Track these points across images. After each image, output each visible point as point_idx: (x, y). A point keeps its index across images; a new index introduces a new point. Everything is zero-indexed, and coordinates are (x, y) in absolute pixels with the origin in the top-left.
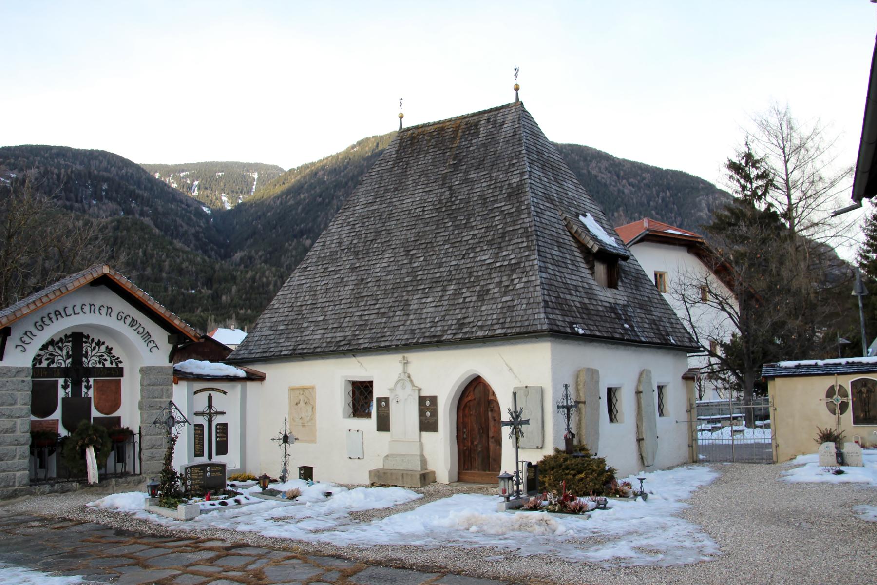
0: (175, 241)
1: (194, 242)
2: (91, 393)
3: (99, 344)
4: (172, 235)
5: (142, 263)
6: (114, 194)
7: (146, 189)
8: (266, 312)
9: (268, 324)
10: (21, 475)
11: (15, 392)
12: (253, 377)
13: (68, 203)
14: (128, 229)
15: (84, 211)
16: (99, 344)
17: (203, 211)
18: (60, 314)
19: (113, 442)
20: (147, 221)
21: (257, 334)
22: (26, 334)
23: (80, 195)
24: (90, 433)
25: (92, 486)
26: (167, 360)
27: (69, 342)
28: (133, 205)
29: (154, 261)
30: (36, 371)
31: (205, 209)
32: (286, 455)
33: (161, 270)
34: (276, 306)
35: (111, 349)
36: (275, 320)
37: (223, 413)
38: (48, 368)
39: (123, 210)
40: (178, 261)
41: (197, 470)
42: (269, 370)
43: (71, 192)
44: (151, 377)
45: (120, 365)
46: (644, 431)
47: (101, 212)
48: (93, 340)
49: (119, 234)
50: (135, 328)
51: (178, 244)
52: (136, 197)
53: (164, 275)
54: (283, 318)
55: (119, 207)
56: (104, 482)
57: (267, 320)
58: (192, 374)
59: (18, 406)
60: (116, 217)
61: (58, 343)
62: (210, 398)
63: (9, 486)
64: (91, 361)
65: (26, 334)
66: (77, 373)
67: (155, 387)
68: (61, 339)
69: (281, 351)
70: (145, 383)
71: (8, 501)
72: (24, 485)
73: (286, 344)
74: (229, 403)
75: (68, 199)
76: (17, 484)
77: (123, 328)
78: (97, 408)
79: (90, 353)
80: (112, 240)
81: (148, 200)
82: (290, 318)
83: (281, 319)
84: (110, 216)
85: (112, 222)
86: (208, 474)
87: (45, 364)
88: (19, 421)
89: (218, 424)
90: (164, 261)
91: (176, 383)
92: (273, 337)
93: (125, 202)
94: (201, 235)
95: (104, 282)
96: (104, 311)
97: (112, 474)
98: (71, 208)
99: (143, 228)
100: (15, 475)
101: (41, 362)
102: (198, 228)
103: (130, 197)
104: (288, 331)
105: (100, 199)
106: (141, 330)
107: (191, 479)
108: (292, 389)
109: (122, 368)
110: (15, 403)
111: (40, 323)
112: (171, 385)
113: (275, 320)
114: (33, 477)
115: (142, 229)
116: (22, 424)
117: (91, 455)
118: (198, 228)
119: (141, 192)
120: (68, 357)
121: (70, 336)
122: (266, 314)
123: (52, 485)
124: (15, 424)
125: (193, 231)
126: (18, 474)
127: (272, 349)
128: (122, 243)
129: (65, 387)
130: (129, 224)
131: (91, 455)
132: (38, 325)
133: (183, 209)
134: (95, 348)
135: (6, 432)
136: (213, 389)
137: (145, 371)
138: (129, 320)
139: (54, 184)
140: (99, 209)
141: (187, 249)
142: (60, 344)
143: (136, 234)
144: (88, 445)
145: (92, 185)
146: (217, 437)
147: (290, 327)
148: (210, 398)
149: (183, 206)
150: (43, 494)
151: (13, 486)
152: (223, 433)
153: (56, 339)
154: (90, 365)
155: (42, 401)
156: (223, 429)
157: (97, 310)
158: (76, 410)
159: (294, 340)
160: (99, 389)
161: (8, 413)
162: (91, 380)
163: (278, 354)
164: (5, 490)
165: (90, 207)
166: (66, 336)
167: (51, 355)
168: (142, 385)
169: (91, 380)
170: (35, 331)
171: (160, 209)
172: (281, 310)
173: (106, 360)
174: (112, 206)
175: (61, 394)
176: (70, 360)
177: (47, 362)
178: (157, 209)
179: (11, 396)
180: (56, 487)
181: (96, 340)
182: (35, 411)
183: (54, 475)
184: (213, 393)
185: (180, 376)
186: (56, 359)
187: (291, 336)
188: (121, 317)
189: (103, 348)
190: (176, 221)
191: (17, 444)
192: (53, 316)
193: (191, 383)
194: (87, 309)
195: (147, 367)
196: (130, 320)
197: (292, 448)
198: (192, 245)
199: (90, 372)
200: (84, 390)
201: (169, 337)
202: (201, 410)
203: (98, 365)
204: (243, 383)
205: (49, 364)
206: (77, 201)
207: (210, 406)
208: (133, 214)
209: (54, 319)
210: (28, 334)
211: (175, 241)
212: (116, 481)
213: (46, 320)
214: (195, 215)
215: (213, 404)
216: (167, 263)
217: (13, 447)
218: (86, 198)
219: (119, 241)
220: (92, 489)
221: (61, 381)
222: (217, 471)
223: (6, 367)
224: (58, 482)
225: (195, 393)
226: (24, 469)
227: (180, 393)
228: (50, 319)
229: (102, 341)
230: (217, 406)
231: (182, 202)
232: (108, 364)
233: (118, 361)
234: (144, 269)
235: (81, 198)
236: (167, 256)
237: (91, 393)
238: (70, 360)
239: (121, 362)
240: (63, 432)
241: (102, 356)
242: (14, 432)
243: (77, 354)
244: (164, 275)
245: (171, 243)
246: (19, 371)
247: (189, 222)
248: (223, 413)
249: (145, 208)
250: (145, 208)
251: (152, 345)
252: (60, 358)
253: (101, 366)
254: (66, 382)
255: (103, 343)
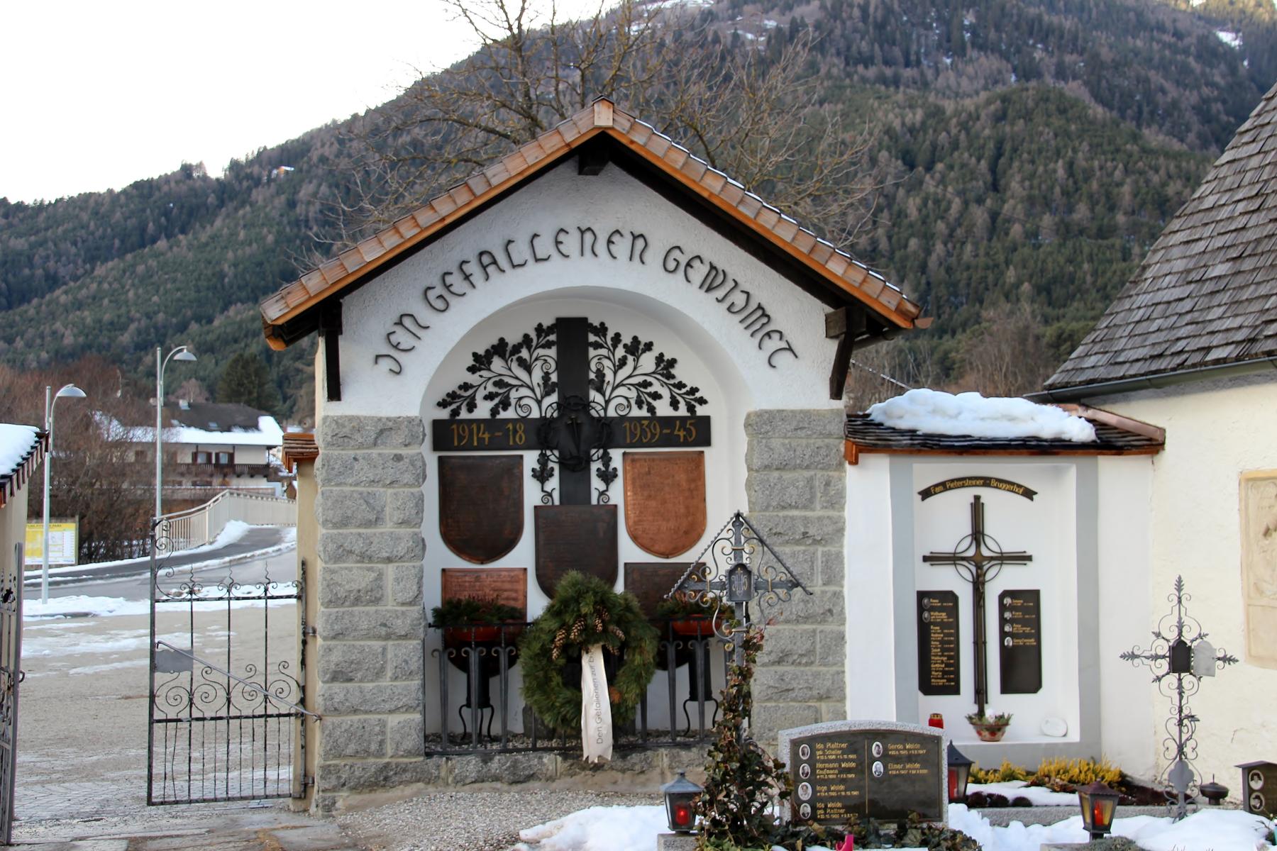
0: (1146, 132)
1: (1196, 127)
2: (617, 494)
3: (636, 348)
4: (1138, 118)
5: (1065, 193)
6: (992, 35)
7: (1068, 10)
8: (1176, 224)
9: (1179, 265)
10: (402, 726)
11: (378, 490)
12: (1110, 442)
13: (889, 72)
14: (1028, 116)
15: (925, 85)
16: (636, 348)
17: (1221, 43)
18: (495, 262)
19: (663, 638)
20: (1074, 89)
21: (1145, 299)
22: (400, 323)
23: (914, 48)
24: (585, 610)
25: (597, 767)
26: (825, 389)
27: (548, 345)
28: (1038, 55)
29: (1095, 185)
30: (443, 434)
31: (1226, 37)
32: (1184, 719)
33: (1112, 208)
34: (1208, 202)
35: (672, 363)
36: (1200, 246)
37: (1024, 558)
38: (492, 423)
39: (1015, 70)
40: (1156, 179)
41: (834, 750)
42: (1177, 417)
43: (894, 43)
44: (776, 443)
45: (701, 411)
46: (1236, 499)
47: (964, 81)
48: (617, 339)
49: (1008, 129)
50: (720, 293)
51: (1154, 137)
52: (1045, 34)
53: (1121, 218)
54: (1228, 239)
55: (1005, 66)
56: (635, 758)
57: (1176, 252)
58: (912, 433)
59: (387, 528)
60: (999, 89)
61: (517, 349)
62: (977, 508)
63: (368, 753)
64: (614, 401)
65: (400, 323)
66: (576, 435)
67: (787, 476)
68: (527, 339)
69: (1208, 349)
70: (757, 463)
71: (367, 797)
72: (409, 753)
73: (1228, 323)
74: (1038, 526)
75: (887, 63)
76: (389, 750)
77: (681, 296)
78: (635, 538)
79: (609, 376)
80: (991, 145)
81: (1076, 38)
82: (1250, 235)
83: (1219, 242)
84: (985, 88)
85: (989, 102)
86: (878, 767)
87: (483, 410)
88: (390, 570)
89: (1005, 594)
90: (1120, 184)
91: (855, 462)
92: (1187, 305)
93: (1018, 51)
94: (1217, 107)
95: (599, 154)
96: (622, 247)
97: (659, 734)
98: (896, 82)
99: (1065, 108)
100: (383, 724)
101: (472, 407)
102: (1206, 91)
103: (1031, 35)
104: (1240, 280)
105: (959, 51)
106: (739, 299)
107: (814, 782)
108: (1251, 481)
109: (707, 419)
110: (378, 521)
111: (439, 290)
112: (840, 466)
113: (1200, 246)
114: (434, 727)
115: (1062, 111)
116: (397, 580)
117: (594, 670)
118: (1206, 91)
119: (1055, 19)
120: (548, 388)
121: (551, 330)
122: (1177, 232)
123: (487, 759)
124: (380, 576)
125: (1193, 98)
126: (393, 721)
127: (1180, 345)
128: (1015, 150)
129: (542, 475)
130: (1031, 104)
131: (594, 670)
132: (432, 295)
133: (1169, 46)
134: (623, 362)
135: (357, 601)
136: (986, 482)
137: (762, 425)
138: (699, 272)
139: (855, 30)
140: (959, 74)
141: (1176, 146)
142: (524, 353)
143: (1047, 125)
144: (583, 646)
145: (939, 18)
146: (1003, 635)
147: (1247, 265)
148: (977, 508)
149: (1167, 38)
150: (460, 781)
151: (380, 753)
152: (1024, 623)
153: (513, 339)
154: (611, 413)
155: (475, 518)
156: (1024, 608)
157: (601, 247)
158: (577, 543)
159: (1256, 306)
160: (640, 484)
161: (358, 546)
162: (616, 455)
163: (1196, 358)
164: (359, 763)
165: (937, 72)
166: (539, 329)
167: (500, 384)
168: (750, 469)
169: (616, 455)
170: (424, 315)
171: (1106, 54)
172: (1224, 213)
173: (656, 396)
174: (989, 63)
175: (532, 495)
176: (554, 398)
177: (490, 404)
178: (1096, 56)
179: (367, 499)
180: (495, 765)
181: (627, 339)
182: (454, 537)
183: (518, 727)
184: (987, 495)
185: (870, 440)
186: (514, 395)
187: (1246, 294)
188: (677, 263)
189: (648, 362)
190: (1147, 80)
191: (388, 637)
192: (472, 268)
193: (904, 462)
194: (571, 243)
195: (760, 414)
196: (705, 269)
197: (1205, 694)
198: (1191, 137)
199: (609, 433)
200: (597, 484)
201: (827, 317)
202: (947, 547)
203: (636, 412)
204: (1085, 461)
205: (494, 411)
206: (907, 64)
207: (978, 534)
208: (1039, 75)
209: (477, 276)
210: (407, 322)
211: (1146, 132)
212: (672, 758)
213: (456, 281)
214: (1199, 57)
215: (988, 529)
216: (1126, 189)
217: (377, 645)
218: (927, 55)
219: (1008, 147)
220: (600, 776)
221: (531, 459)
222: (910, 758)
223: (351, 419)
224: (505, 751)
225: (926, 494)
226: (408, 709)
227: (870, 488)
228: (467, 277)
229: (643, 339)
230: (1000, 535)
231: (1161, 28)
232: (663, 409)
233: (694, 397)
234: (1070, 209)
235: (918, 54)
236: (1127, 171)
237: (617, 494)
238: (554, 398)
239: (702, 401)
240: (536, 604)
241: (646, 384)
242: (377, 601)
243: (573, 382)
244: (1121, 218)
245: (1135, 138)
246: (385, 429)
247: (1183, 77)
248: (1024, 558)
249: (1069, 58)
250: (1069, 58)
251: (774, 343)
252: (524, 392)
253: (644, 413)
254: (543, 460)
255: (649, 346)
